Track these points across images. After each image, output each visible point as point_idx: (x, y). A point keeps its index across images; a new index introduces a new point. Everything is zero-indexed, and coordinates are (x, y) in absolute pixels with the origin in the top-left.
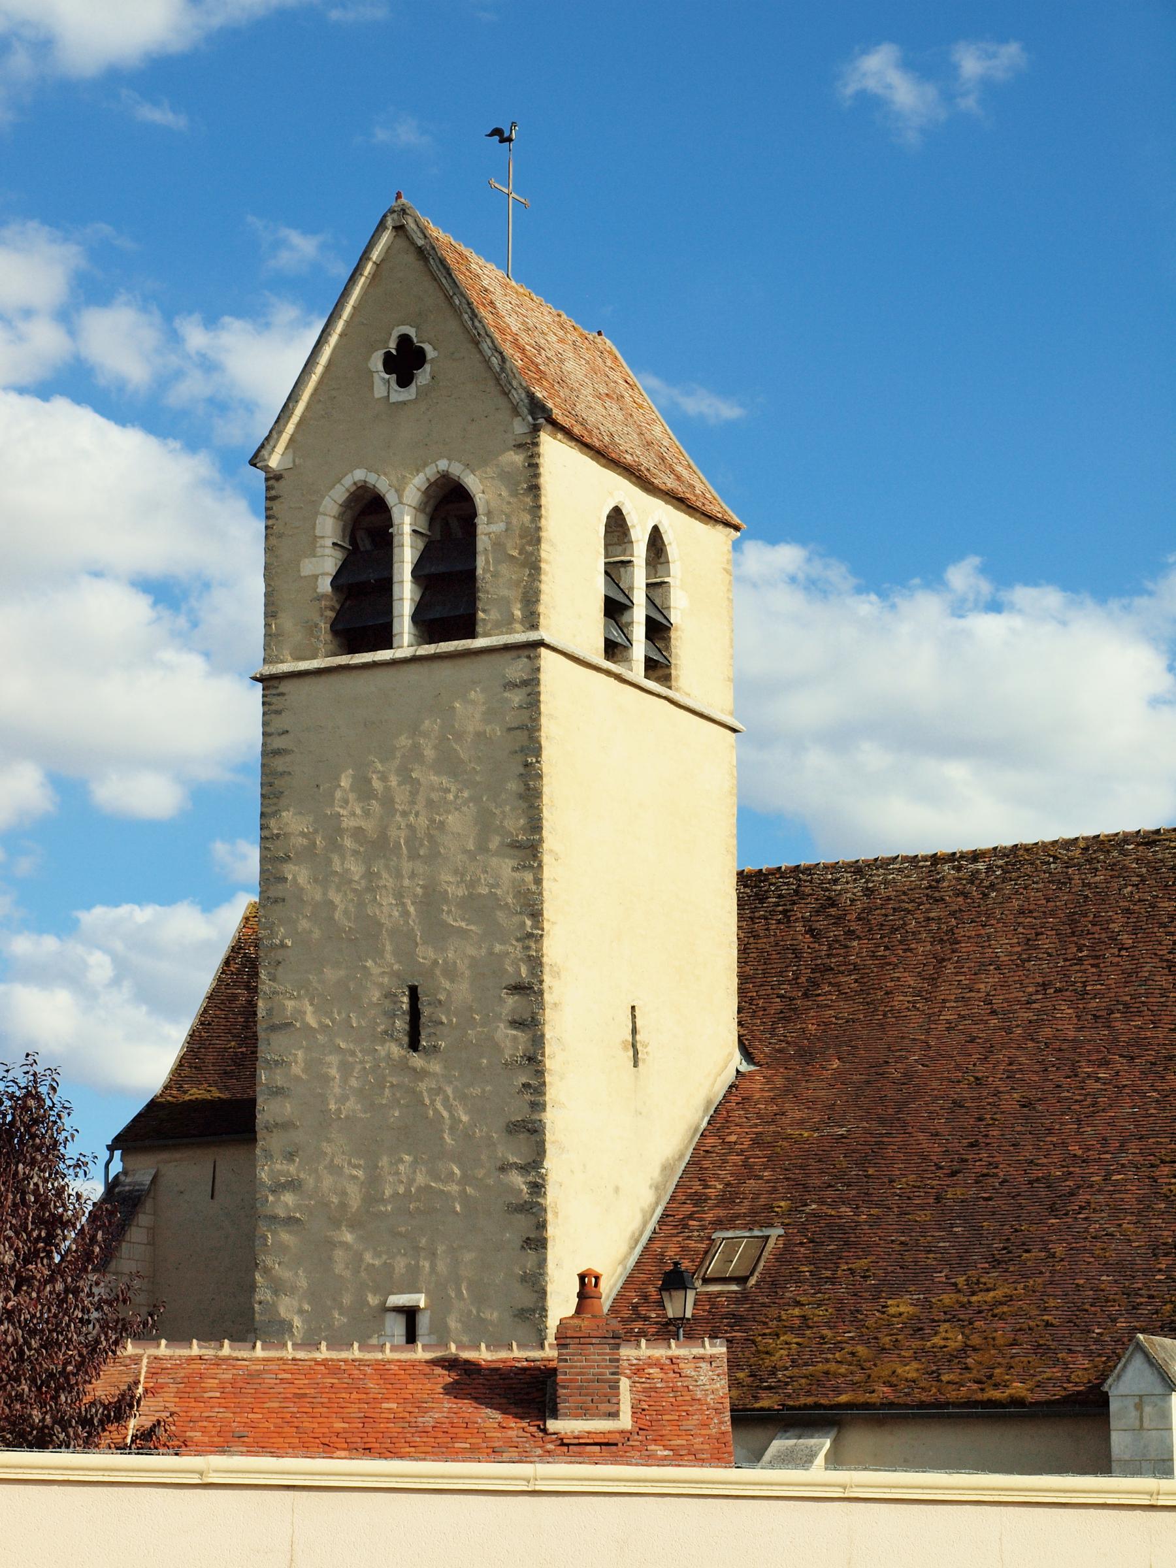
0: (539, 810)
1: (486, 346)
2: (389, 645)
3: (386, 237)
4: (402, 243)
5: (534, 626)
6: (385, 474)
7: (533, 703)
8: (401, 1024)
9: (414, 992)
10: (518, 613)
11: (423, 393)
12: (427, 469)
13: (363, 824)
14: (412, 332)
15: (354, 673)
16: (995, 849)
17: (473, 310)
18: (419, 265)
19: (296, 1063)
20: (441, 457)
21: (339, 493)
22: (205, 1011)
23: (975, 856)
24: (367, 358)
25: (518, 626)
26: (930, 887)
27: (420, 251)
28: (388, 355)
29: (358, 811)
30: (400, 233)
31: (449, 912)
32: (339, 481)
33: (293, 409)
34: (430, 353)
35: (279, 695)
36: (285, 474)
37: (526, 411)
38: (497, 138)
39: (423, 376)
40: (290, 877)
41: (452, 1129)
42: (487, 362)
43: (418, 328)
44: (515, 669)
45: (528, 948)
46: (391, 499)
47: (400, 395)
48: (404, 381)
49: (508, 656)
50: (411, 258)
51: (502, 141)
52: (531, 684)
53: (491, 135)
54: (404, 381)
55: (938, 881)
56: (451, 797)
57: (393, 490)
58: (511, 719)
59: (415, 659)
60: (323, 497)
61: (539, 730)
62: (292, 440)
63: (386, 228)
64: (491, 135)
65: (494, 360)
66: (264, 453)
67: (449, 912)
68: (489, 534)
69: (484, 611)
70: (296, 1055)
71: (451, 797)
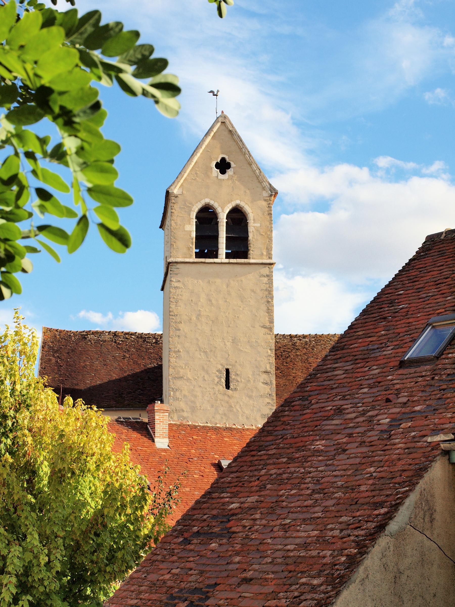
0: (273, 316)
1: (254, 167)
2: (216, 257)
3: (219, 124)
4: (223, 127)
5: (270, 258)
6: (217, 202)
7: (271, 282)
8: (223, 381)
9: (227, 371)
10: (265, 253)
11: (231, 178)
12: (232, 203)
13: (209, 315)
14: (226, 157)
15: (205, 265)
16: (310, 335)
17: (250, 154)
18: (230, 136)
19: (184, 390)
20: (237, 199)
21: (199, 206)
22: (41, 364)
23: (304, 337)
24: (211, 163)
25: (264, 257)
26: (293, 345)
27: (230, 131)
28: (217, 163)
29: (207, 310)
30: (223, 124)
31: (241, 346)
32: (200, 201)
33: (184, 175)
34: (233, 165)
35: (177, 268)
36: (179, 196)
37: (268, 190)
38: (212, 94)
39: (230, 172)
40: (181, 329)
41: (242, 415)
42: (254, 172)
43: (229, 156)
44: (265, 270)
45: (269, 360)
46: (219, 210)
47: (221, 176)
48: (223, 172)
49: (262, 266)
50: (226, 133)
51: (214, 95)
52: (270, 277)
53: (210, 92)
54: (223, 172)
55: (295, 343)
56: (241, 309)
57: (220, 208)
58: (264, 287)
59: (222, 263)
60: (193, 205)
61: (273, 291)
62: (182, 185)
63: (218, 122)
64: (210, 92)
65: (257, 171)
66: (172, 187)
67: (241, 346)
68: (254, 227)
69: (252, 251)
70: (184, 388)
71: (241, 309)
